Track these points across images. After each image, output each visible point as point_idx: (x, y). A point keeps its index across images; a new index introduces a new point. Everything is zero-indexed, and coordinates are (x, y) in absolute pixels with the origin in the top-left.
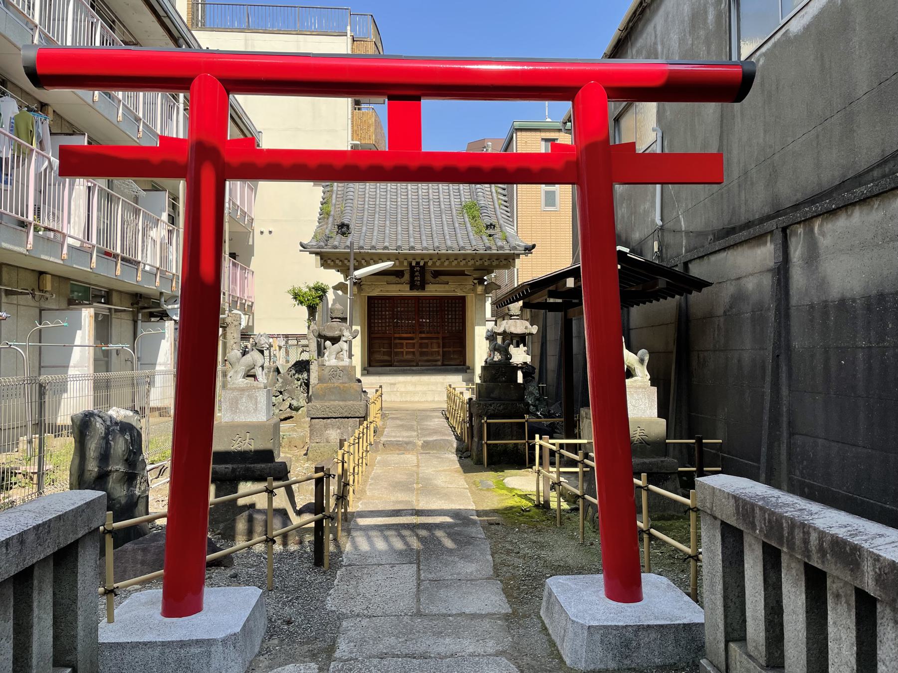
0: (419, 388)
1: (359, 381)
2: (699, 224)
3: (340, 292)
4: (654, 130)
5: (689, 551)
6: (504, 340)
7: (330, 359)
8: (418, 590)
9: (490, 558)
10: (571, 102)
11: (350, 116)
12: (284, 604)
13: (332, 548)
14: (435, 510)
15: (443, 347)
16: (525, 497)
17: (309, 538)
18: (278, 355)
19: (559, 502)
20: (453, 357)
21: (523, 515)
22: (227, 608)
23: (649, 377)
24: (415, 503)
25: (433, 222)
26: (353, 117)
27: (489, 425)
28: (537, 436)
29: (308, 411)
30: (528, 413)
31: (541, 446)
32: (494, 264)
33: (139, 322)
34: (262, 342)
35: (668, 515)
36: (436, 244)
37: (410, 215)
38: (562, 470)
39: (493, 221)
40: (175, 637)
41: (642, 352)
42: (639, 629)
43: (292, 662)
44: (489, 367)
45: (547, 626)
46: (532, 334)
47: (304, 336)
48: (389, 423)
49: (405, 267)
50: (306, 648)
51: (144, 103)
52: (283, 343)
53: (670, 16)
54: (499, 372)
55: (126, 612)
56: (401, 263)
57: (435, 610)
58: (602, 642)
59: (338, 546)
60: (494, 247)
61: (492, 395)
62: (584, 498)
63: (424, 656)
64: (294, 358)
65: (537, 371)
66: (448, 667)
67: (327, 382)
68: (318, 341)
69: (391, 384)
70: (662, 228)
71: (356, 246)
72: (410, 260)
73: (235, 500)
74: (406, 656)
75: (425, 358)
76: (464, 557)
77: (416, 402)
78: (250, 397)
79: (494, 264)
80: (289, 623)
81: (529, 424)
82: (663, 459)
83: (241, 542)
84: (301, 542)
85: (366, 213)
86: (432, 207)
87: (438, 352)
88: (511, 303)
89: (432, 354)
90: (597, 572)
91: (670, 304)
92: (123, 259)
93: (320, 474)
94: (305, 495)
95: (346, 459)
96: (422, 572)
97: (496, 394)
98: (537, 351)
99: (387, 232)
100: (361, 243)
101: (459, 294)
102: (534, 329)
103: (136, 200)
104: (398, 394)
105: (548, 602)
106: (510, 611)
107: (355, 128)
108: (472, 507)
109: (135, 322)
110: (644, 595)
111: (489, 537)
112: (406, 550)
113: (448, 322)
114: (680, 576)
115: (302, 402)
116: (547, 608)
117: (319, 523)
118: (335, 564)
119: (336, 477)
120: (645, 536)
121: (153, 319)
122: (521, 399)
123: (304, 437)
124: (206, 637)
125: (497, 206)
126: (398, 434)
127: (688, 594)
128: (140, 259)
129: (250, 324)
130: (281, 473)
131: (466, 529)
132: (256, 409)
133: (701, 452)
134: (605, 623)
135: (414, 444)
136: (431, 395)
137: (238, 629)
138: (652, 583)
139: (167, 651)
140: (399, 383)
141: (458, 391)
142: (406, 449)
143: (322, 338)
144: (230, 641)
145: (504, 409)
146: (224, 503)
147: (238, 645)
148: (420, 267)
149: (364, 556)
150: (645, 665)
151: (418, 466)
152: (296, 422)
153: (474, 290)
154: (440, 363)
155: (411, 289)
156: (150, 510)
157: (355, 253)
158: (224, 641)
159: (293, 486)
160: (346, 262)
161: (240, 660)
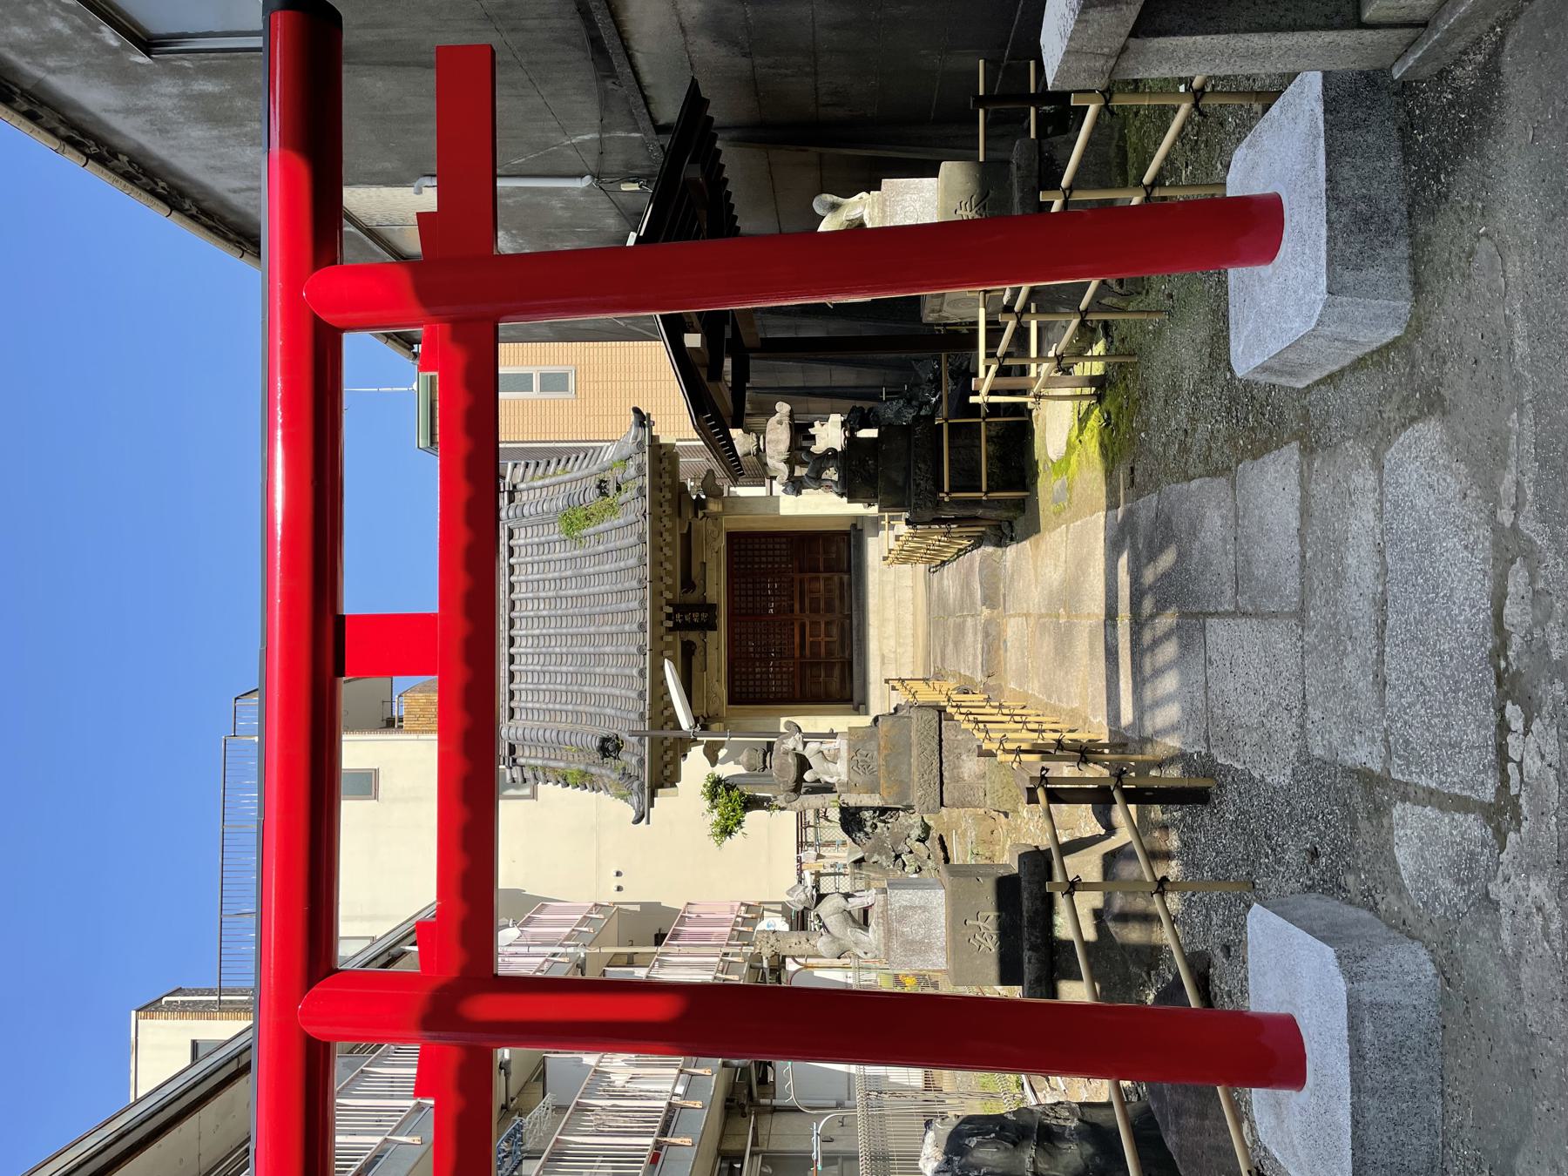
0: (890, 614)
1: (876, 720)
2: (588, 108)
3: (722, 753)
4: (419, 192)
5: (1185, 108)
6: (803, 464)
7: (837, 772)
8: (1256, 615)
9: (1195, 484)
10: (345, 335)
11: (414, 736)
12: (1279, 862)
13: (1174, 772)
14: (1107, 585)
15: (817, 571)
16: (1083, 421)
17: (1156, 812)
18: (832, 861)
19: (1093, 358)
20: (835, 553)
21: (1117, 425)
22: (1287, 969)
23: (863, 194)
24: (1093, 621)
25: (597, 589)
26: (415, 731)
27: (953, 489)
28: (973, 399)
29: (928, 811)
30: (932, 418)
31: (991, 393)
33: (775, 1102)
34: (803, 897)
35: (1115, 157)
36: (635, 584)
37: (585, 630)
38: (1033, 353)
39: (593, 483)
40: (1345, 1070)
41: (818, 207)
42: (1334, 197)
43: (1391, 850)
44: (850, 491)
45: (1325, 373)
47: (801, 816)
48: (950, 666)
49: (675, 639)
50: (1363, 825)
51: (392, 1097)
52: (812, 852)
53: (212, 162)
54: (857, 471)
55: (1295, 1155)
56: (669, 646)
57: (1293, 584)
58: (1358, 268)
59: (1171, 761)
60: (639, 482)
61: (900, 483)
62: (1086, 311)
63: (1382, 604)
64: (836, 832)
65: (858, 404)
66: (1403, 559)
67: (878, 778)
68: (807, 792)
69: (883, 663)
70: (597, 176)
71: (639, 727)
72: (663, 630)
73: (1086, 944)
74: (1380, 637)
75: (837, 603)
76: (1194, 531)
77: (915, 619)
78: (902, 919)
79: (668, 481)
80: (1315, 854)
82: (1014, 168)
83: (1164, 935)
84: (1165, 827)
85: (581, 708)
87: (826, 579)
88: (733, 449)
89: (828, 591)
90: (1222, 283)
91: (734, 160)
92: (664, 1133)
93: (1041, 794)
94: (1080, 820)
95: (1014, 746)
96: (1221, 609)
97: (899, 478)
98: (824, 403)
99: (614, 670)
100: (634, 716)
101: (724, 543)
102: (783, 408)
103: (560, 1109)
105: (1281, 373)
106: (1295, 444)
108: (1100, 517)
109: (775, 1110)
110: (1269, 191)
111: (1157, 485)
112: (1180, 637)
113: (773, 563)
114: (1230, 128)
115: (915, 819)
116: (1290, 374)
117: (1130, 797)
118: (1208, 766)
119: (1045, 764)
120: (1157, 193)
121: (770, 1079)
122: (907, 430)
123: (975, 817)
124: (1344, 1011)
125: (567, 477)
126: (971, 650)
127: (1266, 109)
128: (664, 1104)
129: (779, 908)
130: (1038, 862)
131: (1141, 529)
132: (924, 909)
133: (1003, 98)
134: (1323, 262)
135: (989, 622)
136: (902, 591)
137: (1329, 952)
138: (1245, 174)
139: (1369, 1084)
140: (881, 649)
141: (893, 545)
142: (999, 638)
143: (798, 787)
144: (1351, 966)
145: (925, 462)
146: (1091, 968)
147: (1358, 952)
148: (675, 612)
149: (1190, 714)
150: (1402, 186)
151: (1027, 615)
152: (949, 830)
153: (716, 517)
154: (846, 577)
155: (714, 628)
156: (1104, 1100)
157: (652, 728)
158: (1352, 977)
159: (1063, 839)
160: (667, 743)
161: (1388, 948)
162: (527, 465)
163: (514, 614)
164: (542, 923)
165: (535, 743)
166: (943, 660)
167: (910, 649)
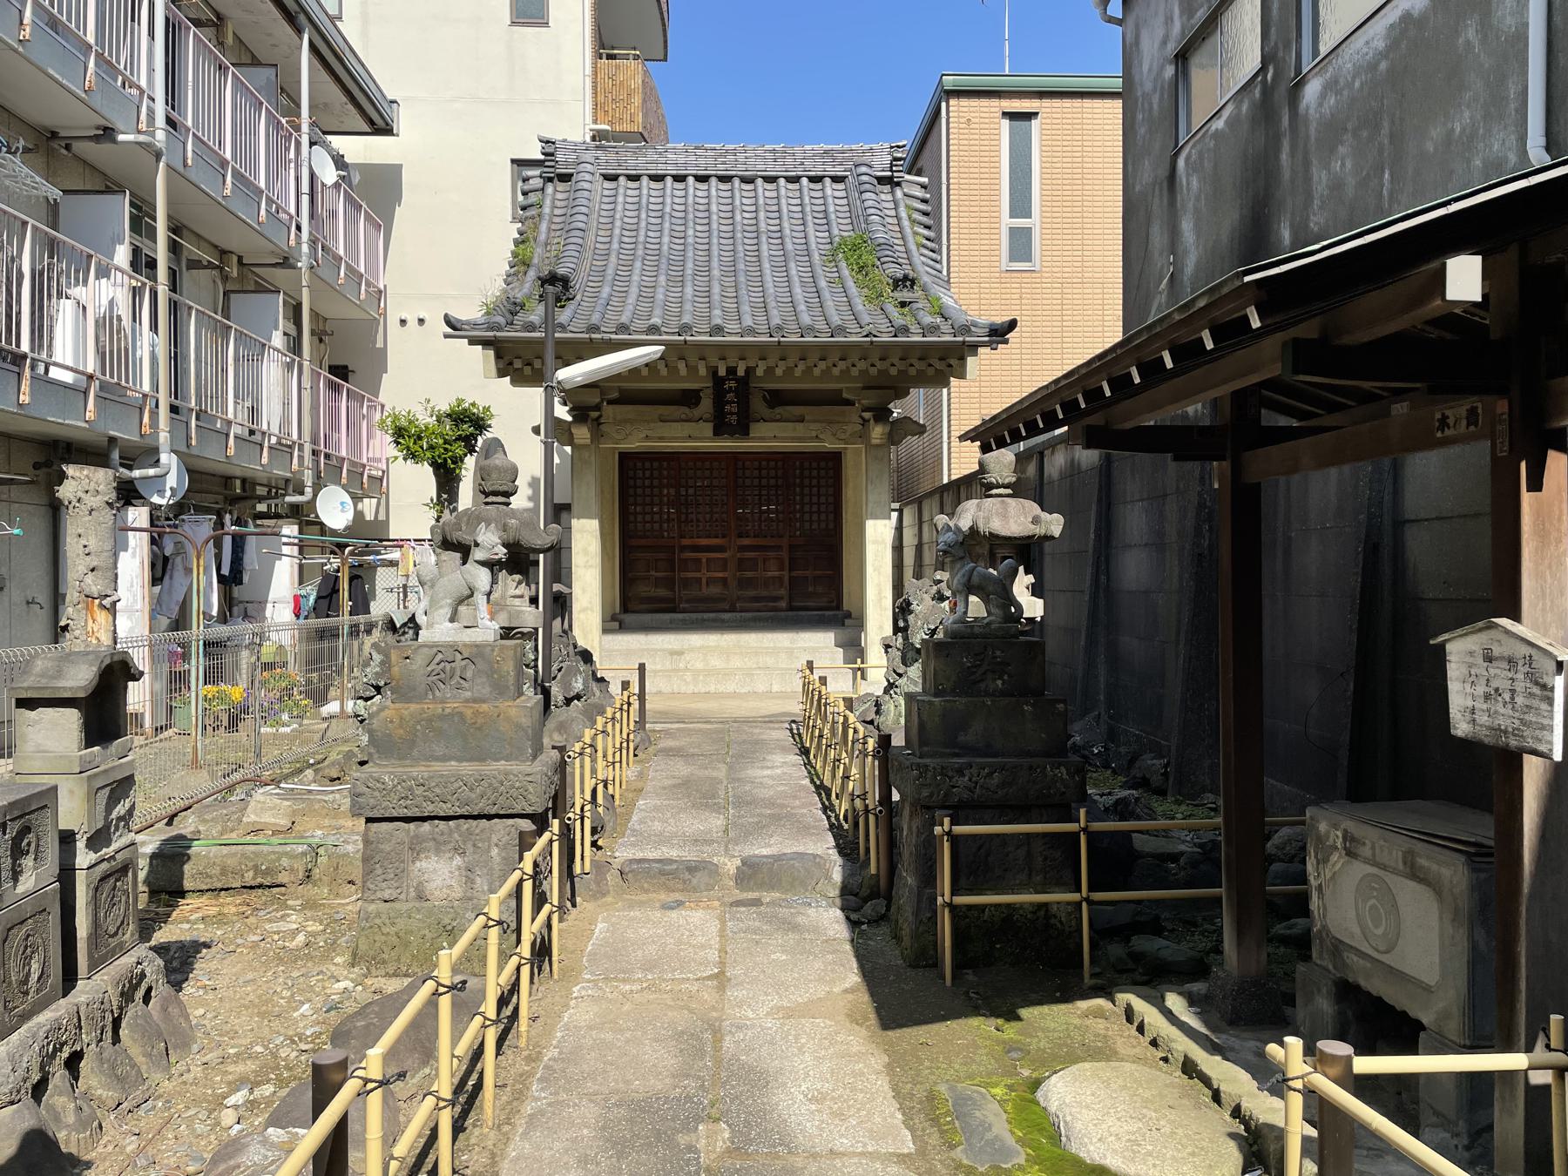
0: (736, 662)
11: (589, 70)
15: (790, 570)
27: (955, 840)
32: (912, 371)
36: (776, 321)
37: (715, 263)
46: (1052, 538)
48: (662, 772)
49: (701, 382)
61: (962, 738)
67: (420, 698)
69: (673, 653)
75: (751, 593)
81: (1093, 837)
85: (613, 259)
86: (764, 247)
87: (780, 578)
99: (660, 296)
102: (1054, 524)
104: (688, 676)
107: (601, 98)
125: (913, 247)
129: (382, 517)
135: (712, 870)
140: (692, 650)
148: (737, 380)
151: (721, 980)
153: (864, 436)
154: (783, 604)
155: (718, 432)
162: (924, 201)
163: (737, 181)
164: (351, 223)
165: (571, 203)
166: (670, 753)
167: (691, 689)
